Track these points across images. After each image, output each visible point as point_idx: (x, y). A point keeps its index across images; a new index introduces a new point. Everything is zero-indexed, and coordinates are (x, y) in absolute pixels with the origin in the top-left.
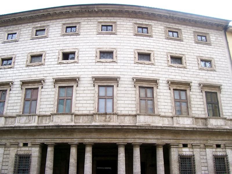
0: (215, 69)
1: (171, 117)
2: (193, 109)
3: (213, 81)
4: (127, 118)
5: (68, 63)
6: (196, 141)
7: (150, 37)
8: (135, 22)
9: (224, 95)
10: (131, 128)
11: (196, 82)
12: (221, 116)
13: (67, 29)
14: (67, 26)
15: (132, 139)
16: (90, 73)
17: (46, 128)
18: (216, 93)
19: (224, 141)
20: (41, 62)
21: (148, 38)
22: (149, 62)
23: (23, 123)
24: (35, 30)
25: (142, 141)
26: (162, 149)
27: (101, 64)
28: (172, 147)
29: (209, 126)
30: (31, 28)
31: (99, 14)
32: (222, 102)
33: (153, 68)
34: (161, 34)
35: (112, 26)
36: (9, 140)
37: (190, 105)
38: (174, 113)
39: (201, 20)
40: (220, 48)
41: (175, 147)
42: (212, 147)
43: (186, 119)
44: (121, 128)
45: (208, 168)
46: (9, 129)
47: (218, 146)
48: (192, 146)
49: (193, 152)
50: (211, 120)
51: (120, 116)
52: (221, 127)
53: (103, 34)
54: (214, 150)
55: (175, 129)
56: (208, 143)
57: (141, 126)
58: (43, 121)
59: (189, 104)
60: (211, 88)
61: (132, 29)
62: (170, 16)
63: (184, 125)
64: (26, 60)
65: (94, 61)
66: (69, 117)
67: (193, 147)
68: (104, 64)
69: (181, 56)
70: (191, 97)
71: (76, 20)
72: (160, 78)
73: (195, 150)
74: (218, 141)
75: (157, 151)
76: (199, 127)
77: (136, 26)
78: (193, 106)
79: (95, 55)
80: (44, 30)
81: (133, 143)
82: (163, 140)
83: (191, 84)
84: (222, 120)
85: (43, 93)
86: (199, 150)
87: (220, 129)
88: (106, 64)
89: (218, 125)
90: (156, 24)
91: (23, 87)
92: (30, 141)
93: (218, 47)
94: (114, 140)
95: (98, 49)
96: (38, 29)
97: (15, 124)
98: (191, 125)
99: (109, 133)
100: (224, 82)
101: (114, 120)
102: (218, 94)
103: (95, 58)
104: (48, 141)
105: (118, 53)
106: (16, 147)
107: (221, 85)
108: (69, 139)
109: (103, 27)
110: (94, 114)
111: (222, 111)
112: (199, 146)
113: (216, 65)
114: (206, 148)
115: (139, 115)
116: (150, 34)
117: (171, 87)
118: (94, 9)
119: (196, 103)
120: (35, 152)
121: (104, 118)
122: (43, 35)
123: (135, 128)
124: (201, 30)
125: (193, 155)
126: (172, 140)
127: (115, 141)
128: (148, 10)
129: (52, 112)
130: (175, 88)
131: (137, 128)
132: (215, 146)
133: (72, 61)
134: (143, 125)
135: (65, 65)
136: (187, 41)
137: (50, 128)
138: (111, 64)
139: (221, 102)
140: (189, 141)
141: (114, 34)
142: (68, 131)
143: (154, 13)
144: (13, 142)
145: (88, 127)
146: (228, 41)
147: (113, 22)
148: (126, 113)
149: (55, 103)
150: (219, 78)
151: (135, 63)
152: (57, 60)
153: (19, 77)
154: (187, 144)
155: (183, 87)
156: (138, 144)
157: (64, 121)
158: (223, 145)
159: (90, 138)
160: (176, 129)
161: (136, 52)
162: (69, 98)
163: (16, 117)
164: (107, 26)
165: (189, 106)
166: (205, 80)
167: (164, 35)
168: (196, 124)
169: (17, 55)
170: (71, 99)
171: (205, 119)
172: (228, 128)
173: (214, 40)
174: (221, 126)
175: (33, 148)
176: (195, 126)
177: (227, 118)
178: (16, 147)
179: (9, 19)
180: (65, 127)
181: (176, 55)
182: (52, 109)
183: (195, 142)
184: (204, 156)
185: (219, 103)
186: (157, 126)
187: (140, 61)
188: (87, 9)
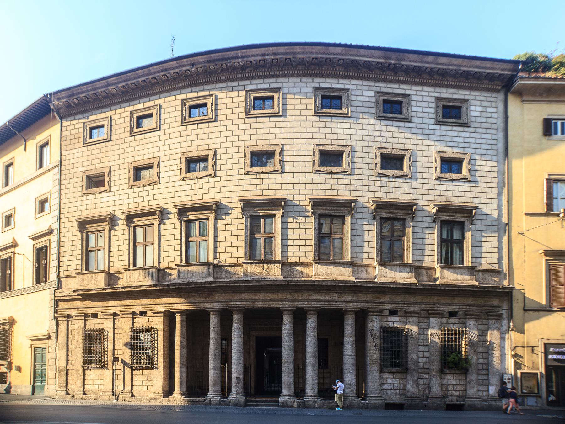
6: (412, 306)
7: (405, 122)
8: (317, 85)
13: (192, 110)
16: (235, 194)
17: (171, 287)
19: (464, 307)
25: (320, 305)
28: (370, 314)
31: (248, 72)
33: (343, 180)
39: (455, 68)
44: (286, 284)
47: (452, 314)
48: (406, 313)
52: (463, 283)
55: (378, 286)
57: (319, 281)
58: (166, 278)
62: (390, 64)
68: (258, 176)
71: (273, 83)
72: (357, 198)
74: (454, 307)
75: (345, 320)
86: (417, 320)
87: (459, 286)
88: (263, 176)
90: (359, 87)
94: (277, 303)
98: (407, 280)
99: (268, 292)
108: (207, 303)
109: (256, 102)
114: (429, 318)
118: (237, 61)
120: (158, 323)
123: (310, 284)
124: (440, 93)
128: (344, 52)
130: (384, 214)
132: (446, 314)
133: (205, 173)
134: (322, 278)
135: (193, 182)
136: (420, 120)
137: (177, 287)
138: (272, 176)
142: (205, 291)
143: (356, 60)
145: (234, 283)
146: (509, 114)
147: (275, 88)
155: (400, 213)
160: (380, 286)
161: (317, 150)
166: (444, 198)
168: (416, 278)
173: (477, 114)
174: (464, 280)
179: (85, 96)
180: (199, 285)
181: (394, 152)
183: (411, 308)
186: (346, 281)
188: (224, 62)
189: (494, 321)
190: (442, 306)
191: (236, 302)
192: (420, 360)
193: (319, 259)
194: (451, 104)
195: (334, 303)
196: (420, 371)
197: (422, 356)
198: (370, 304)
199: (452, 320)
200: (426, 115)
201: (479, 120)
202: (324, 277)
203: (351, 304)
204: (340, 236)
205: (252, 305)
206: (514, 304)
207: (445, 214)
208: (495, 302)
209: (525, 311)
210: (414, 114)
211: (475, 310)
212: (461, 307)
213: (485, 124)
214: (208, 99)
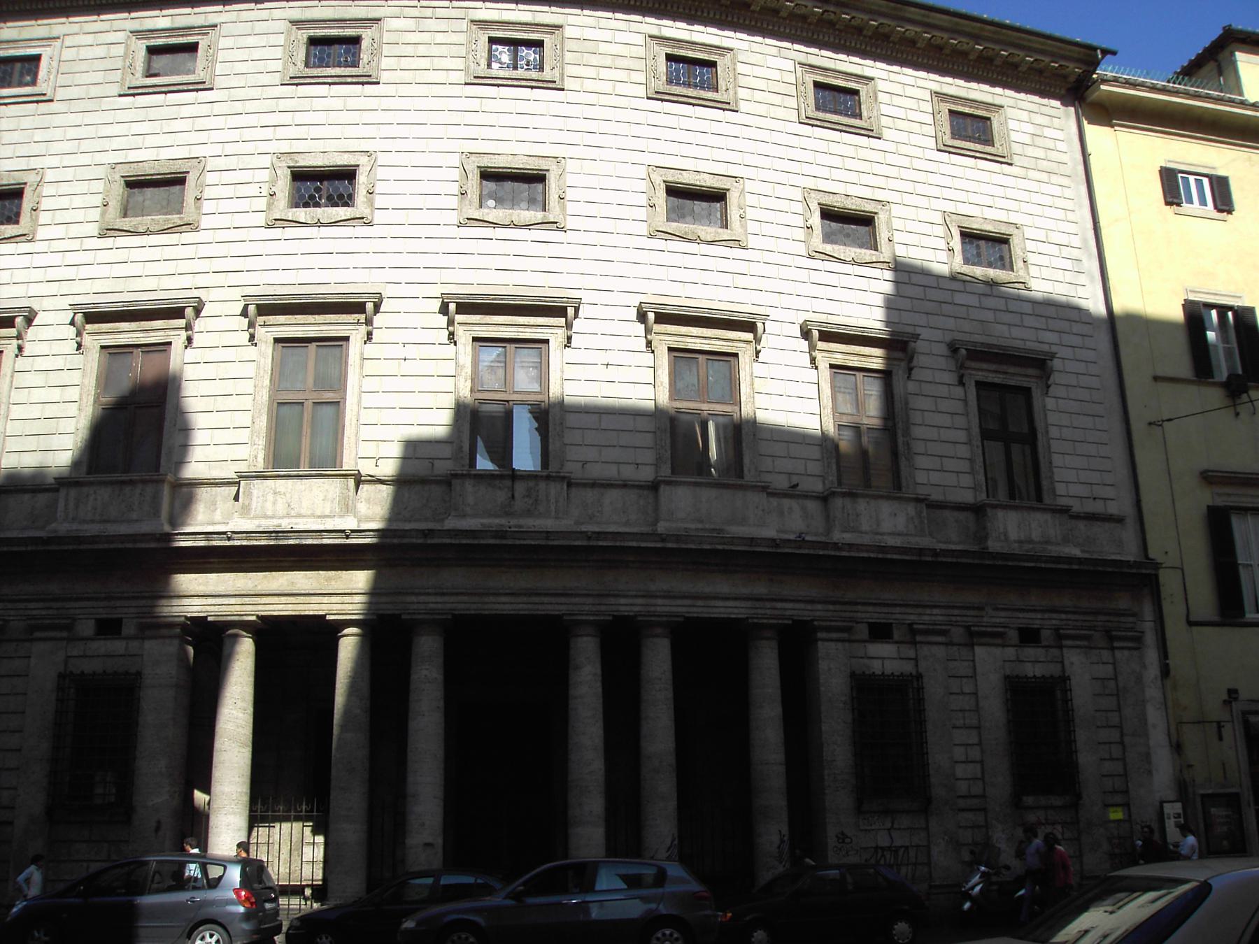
0: (1026, 279)
1: (817, 498)
2: (921, 461)
3: (1016, 332)
4: (612, 496)
5: (319, 224)
6: (928, 611)
8: (655, 32)
9: (1060, 401)
10: (634, 544)
11: (938, 335)
12: (1047, 499)
14: (312, 33)
15: (636, 596)
18: (1029, 389)
19: (1055, 616)
20: (180, 213)
21: (863, 141)
22: (721, 230)
23: (93, 521)
24: (140, 47)
25: (680, 609)
26: (774, 644)
27: (488, 232)
28: (820, 635)
29: (994, 545)
30: (120, 36)
32: (1054, 432)
34: (777, 99)
35: (539, 44)
36: (22, 605)
37: (908, 444)
38: (832, 478)
40: (1054, 179)
41: (834, 635)
42: (999, 641)
43: (886, 508)
45: (980, 735)
46: (23, 549)
47: (1029, 636)
49: (916, 660)
50: (1000, 514)
51: (578, 485)
53: (495, 81)
54: (1010, 652)
55: (838, 554)
56: (985, 619)
57: (678, 538)
59: (900, 440)
60: (1004, 368)
61: (641, 65)
63: (880, 537)
64: (98, 200)
65: (453, 218)
66: (332, 488)
67: (918, 638)
69: (870, 207)
70: (911, 406)
73: (925, 651)
76: (944, 546)
77: (662, 51)
78: (918, 447)
79: (455, 188)
80: (192, 48)
81: (640, 618)
82: (779, 605)
83: (912, 344)
84: (1048, 516)
85: (20, 380)
87: (1038, 559)
89: (1030, 541)
91: (85, 336)
92: (133, 610)
93: (1044, 177)
95: (473, 158)
96: (160, 42)
97: (54, 525)
100: (1067, 339)
101: (553, 507)
102: (1036, 394)
103: (454, 202)
104: (224, 608)
105: (570, 180)
106: (62, 639)
107: (1053, 356)
110: (455, 476)
111: (1051, 477)
112: (943, 633)
113: (1032, 258)
114: (972, 645)
115: (669, 483)
116: (725, 96)
117: (818, 355)
119: (932, 434)
121: (501, 496)
122: (188, 72)
125: (914, 673)
126: (819, 602)
127: (557, 607)
129: (243, 467)
131: (659, 545)
132: (1013, 635)
139: (1047, 432)
140: (898, 610)
141: (549, 85)
144: (44, 612)
146: (1090, 149)
148: (610, 472)
149: (257, 422)
150: (1040, 323)
151: (651, 236)
152: (262, 204)
153: (65, 288)
154: (891, 624)
156: (665, 619)
157: (303, 512)
158: (1049, 632)
159: (436, 594)
160: (844, 554)
161: (658, 179)
162: (329, 396)
163: (57, 490)
164: (514, 43)
165: (901, 448)
167: (793, 102)
169: (50, 175)
170: (338, 405)
171: (978, 510)
172: (1076, 552)
175: (149, 645)
176: (925, 542)
177: (1074, 509)
178: (62, 639)
182: (243, 452)
183: (926, 618)
184: (965, 680)
185: (1039, 436)
186: (752, 539)
187: (674, 224)
189: (1126, 653)
190: (1003, 614)
191: (428, 594)
192: (960, 771)
193: (673, 472)
194: (967, 110)
195: (720, 603)
196: (962, 803)
197: (963, 758)
198: (819, 607)
199: (1031, 652)
200: (916, 128)
201: (1030, 151)
202: (693, 526)
203: (768, 605)
204: (915, 340)
205: (474, 606)
206: (1167, 608)
207: (984, 366)
208: (1123, 602)
209: (1191, 624)
210: (884, 121)
211: (1079, 624)
212: (1046, 616)
213: (1045, 163)
214: (366, 27)
